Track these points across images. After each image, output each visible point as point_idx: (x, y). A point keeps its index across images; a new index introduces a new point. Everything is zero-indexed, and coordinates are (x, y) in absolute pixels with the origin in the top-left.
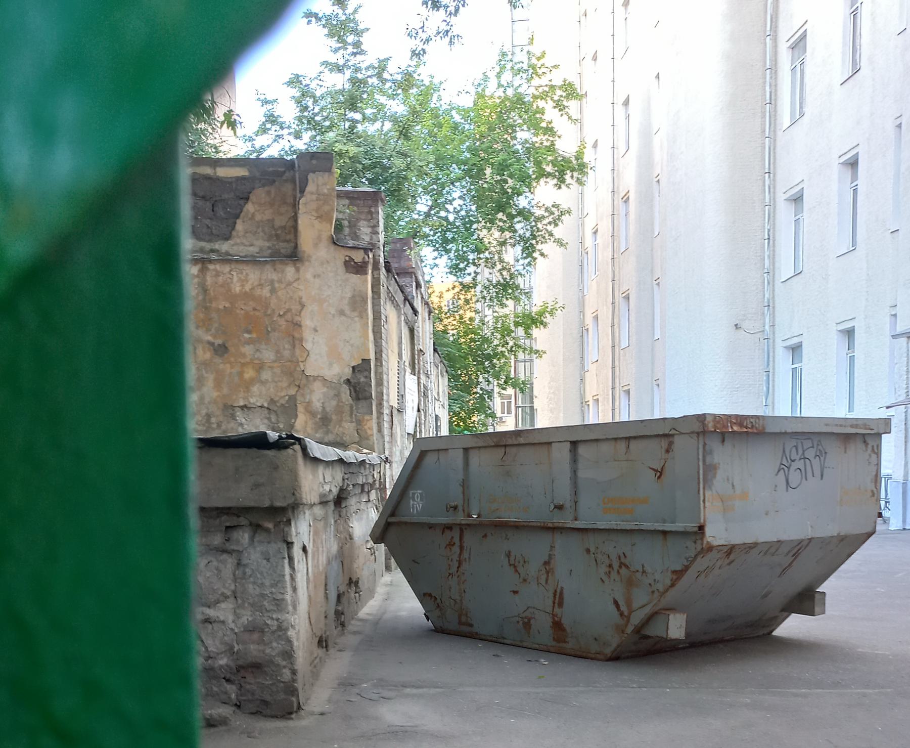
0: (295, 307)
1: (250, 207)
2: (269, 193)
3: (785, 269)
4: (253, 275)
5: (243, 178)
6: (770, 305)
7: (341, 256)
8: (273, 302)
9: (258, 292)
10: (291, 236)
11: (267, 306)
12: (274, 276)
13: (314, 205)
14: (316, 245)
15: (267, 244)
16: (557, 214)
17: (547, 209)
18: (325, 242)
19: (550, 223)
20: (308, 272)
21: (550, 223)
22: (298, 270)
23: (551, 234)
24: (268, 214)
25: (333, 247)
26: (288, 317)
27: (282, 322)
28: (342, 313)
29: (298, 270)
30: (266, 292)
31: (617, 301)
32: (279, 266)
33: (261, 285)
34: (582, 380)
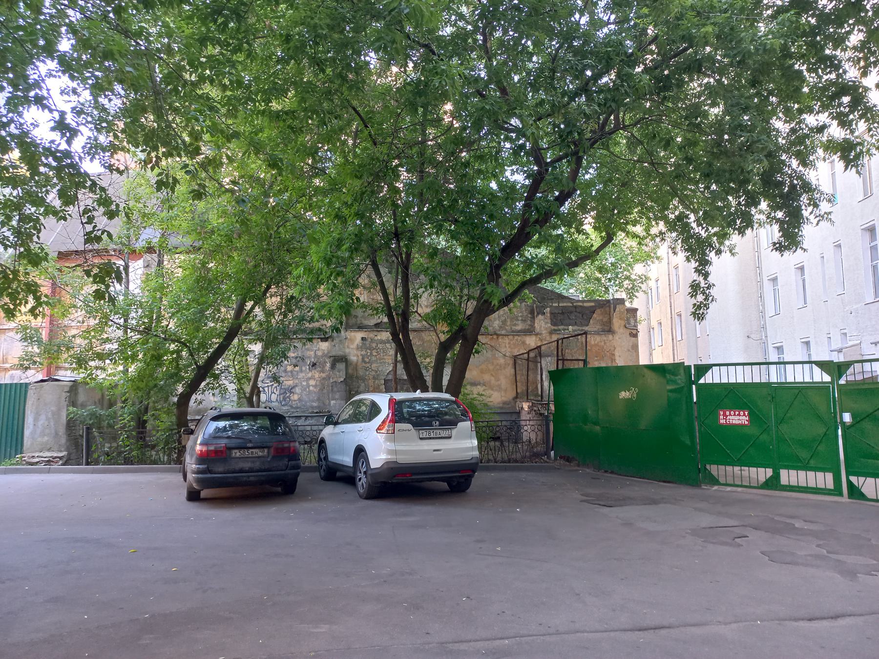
0: (612, 349)
1: (595, 315)
3: (770, 311)
4: (598, 338)
5: (592, 306)
6: (764, 327)
7: (628, 331)
9: (600, 344)
11: (603, 348)
12: (605, 338)
16: (645, 279)
18: (622, 327)
20: (617, 337)
23: (640, 288)
27: (608, 354)
28: (629, 350)
30: (603, 343)
31: (673, 316)
34: (651, 354)
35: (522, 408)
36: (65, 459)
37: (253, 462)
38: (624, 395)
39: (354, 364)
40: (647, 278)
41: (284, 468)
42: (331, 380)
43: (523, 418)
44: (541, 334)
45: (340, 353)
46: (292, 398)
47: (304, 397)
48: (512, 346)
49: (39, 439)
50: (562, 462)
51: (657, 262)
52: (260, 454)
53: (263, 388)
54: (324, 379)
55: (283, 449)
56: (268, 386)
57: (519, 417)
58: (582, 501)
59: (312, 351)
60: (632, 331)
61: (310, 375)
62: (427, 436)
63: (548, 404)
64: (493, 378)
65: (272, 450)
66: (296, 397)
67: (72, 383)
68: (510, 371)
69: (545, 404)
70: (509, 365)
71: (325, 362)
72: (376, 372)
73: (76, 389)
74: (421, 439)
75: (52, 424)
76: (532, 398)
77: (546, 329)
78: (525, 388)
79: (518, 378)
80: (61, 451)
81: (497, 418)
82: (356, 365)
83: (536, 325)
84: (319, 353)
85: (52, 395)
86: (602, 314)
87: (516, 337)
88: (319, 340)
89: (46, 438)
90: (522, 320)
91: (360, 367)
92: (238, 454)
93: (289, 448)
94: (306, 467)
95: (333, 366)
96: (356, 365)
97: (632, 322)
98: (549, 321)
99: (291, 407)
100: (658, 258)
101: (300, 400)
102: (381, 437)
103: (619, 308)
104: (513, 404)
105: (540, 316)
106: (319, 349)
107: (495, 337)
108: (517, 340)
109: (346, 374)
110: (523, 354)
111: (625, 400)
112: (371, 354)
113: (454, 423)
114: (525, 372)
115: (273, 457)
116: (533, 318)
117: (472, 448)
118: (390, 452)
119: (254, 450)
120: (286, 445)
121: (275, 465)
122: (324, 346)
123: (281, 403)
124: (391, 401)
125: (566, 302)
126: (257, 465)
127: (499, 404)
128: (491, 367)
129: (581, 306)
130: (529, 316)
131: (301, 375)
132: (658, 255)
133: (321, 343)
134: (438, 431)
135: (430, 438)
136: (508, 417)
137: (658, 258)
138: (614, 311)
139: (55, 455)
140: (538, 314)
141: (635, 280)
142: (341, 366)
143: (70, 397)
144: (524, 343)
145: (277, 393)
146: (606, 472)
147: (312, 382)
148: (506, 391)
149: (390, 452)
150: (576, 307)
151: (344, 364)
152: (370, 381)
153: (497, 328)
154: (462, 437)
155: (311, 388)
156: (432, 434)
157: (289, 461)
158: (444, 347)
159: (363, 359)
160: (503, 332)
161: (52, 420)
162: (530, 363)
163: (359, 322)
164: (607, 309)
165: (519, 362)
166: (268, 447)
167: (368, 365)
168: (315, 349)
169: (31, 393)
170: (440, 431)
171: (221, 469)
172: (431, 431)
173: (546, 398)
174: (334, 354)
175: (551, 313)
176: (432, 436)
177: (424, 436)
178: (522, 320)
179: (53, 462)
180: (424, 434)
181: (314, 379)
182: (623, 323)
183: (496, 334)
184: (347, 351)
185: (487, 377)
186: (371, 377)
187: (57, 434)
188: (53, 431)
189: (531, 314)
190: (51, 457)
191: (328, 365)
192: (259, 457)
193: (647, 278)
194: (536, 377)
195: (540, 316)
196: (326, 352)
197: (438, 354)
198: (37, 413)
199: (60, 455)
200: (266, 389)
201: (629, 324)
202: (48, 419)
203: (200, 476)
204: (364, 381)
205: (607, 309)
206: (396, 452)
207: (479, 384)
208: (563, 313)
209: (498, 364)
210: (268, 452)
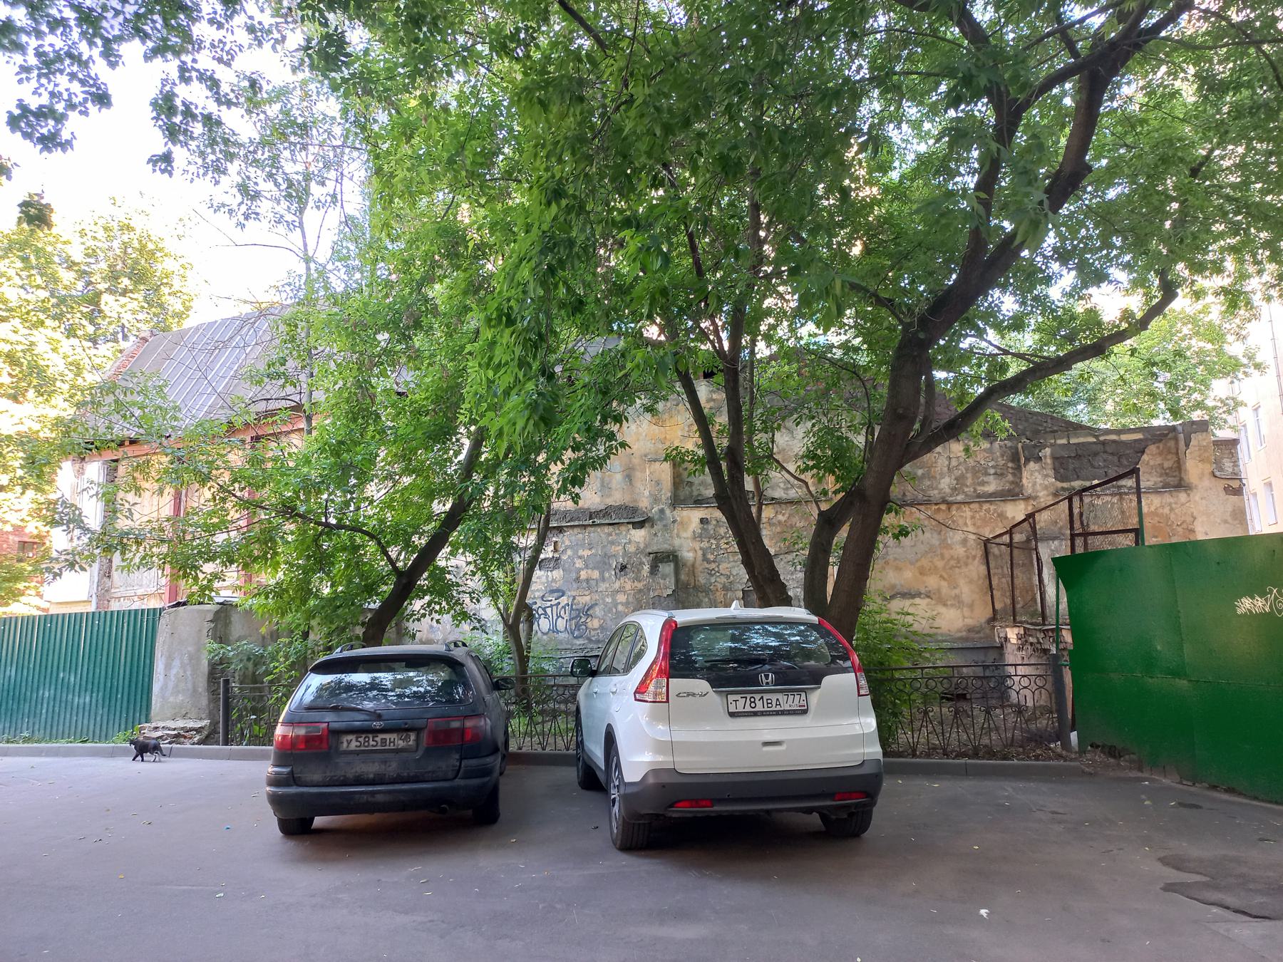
0: (1189, 519)
1: (1145, 457)
2: (1158, 448)
5: (1140, 440)
7: (1223, 483)
8: (1172, 516)
9: (1161, 511)
10: (1177, 473)
12: (1172, 500)
13: (1197, 453)
14: (1201, 479)
15: (1159, 479)
17: (1222, 401)
19: (1224, 412)
20: (1196, 496)
21: (1224, 412)
22: (1189, 495)
23: (1225, 422)
24: (1159, 460)
25: (1214, 479)
26: (1184, 526)
28: (1226, 522)
29: (1189, 495)
30: (1167, 510)
32: (1174, 494)
33: (1163, 507)
35: (1006, 639)
36: (205, 733)
37: (385, 762)
38: (1246, 604)
39: (689, 564)
40: (1238, 404)
41: (450, 775)
42: (652, 594)
43: (1010, 658)
44: (1035, 498)
45: (665, 547)
46: (589, 625)
47: (609, 622)
48: (979, 523)
49: (171, 699)
50: (1099, 757)
51: (1256, 373)
52: (401, 744)
53: (544, 609)
54: (640, 591)
55: (448, 733)
56: (551, 606)
57: (1002, 655)
58: (1170, 888)
59: (619, 544)
60: (1231, 483)
61: (617, 585)
62: (748, 709)
63: (1058, 630)
64: (944, 584)
65: (424, 735)
66: (595, 623)
67: (219, 606)
68: (978, 568)
69: (1052, 630)
70: (974, 557)
71: (642, 563)
72: (728, 577)
73: (228, 617)
74: (732, 715)
75: (189, 673)
76: (1024, 619)
77: (1046, 488)
78: (1008, 601)
79: (995, 582)
80: (201, 719)
81: (954, 660)
82: (693, 566)
83: (1024, 481)
84: (632, 549)
85: (193, 623)
86: (1160, 454)
87: (986, 506)
88: (631, 526)
89: (180, 697)
90: (995, 474)
91: (700, 569)
92: (354, 745)
93: (462, 731)
94: (549, 755)
95: (654, 569)
96: (693, 566)
97: (1228, 465)
98: (1051, 473)
99: (589, 639)
100: (1258, 366)
101: (601, 627)
102: (642, 711)
103: (1196, 439)
104: (987, 631)
105: (1032, 464)
106: (630, 542)
107: (943, 507)
108: (988, 511)
109: (677, 581)
110: (1000, 535)
111: (1250, 616)
112: (718, 546)
113: (815, 679)
114: (1007, 571)
115: (428, 752)
116: (1018, 469)
117: (862, 739)
118: (660, 747)
119: (387, 736)
120: (455, 724)
121: (430, 768)
122: (639, 535)
123: (573, 633)
124: (669, 625)
125: (1086, 436)
126: (392, 768)
127: (959, 630)
128: (940, 564)
129: (1114, 441)
130: (1010, 465)
131: (603, 586)
132: (1258, 360)
133: (633, 532)
134: (774, 697)
135: (755, 714)
136: (979, 657)
137: (1258, 366)
138: (1187, 445)
139: (191, 724)
140: (1027, 460)
141: (1215, 408)
142: (667, 569)
143: (215, 629)
144: (1002, 516)
145: (566, 617)
146: (1214, 787)
147: (621, 598)
148: (971, 606)
149: (660, 747)
150: (1104, 443)
151: (672, 565)
152: (718, 594)
153: (948, 490)
154: (835, 709)
155: (620, 608)
156: (759, 704)
157: (461, 760)
158: (828, 523)
159: (704, 555)
160: (960, 498)
161: (189, 668)
162: (1016, 552)
163: (695, 493)
164: (1172, 444)
165: (995, 550)
166: (418, 730)
167: (713, 566)
168: (624, 541)
169: (163, 626)
170: (780, 696)
171: (317, 777)
172: (757, 697)
173: (1052, 620)
174: (654, 548)
175: (1054, 458)
176: (759, 707)
177: (740, 709)
178: (995, 474)
179: (185, 737)
180: (740, 703)
181: (625, 592)
182: (1208, 468)
183: (944, 501)
184: (677, 542)
185: (932, 582)
186: (720, 586)
187: (195, 691)
188: (190, 686)
189: (1012, 461)
190: (182, 728)
191: (646, 568)
192: (397, 751)
193: (1238, 404)
194: (1030, 579)
195: (1032, 464)
196: (642, 546)
197: (817, 534)
198: (170, 656)
199: (198, 725)
200: (549, 610)
201: (1221, 469)
202: (183, 666)
203: (280, 790)
204: (707, 595)
205: (1172, 444)
206: (671, 747)
207: (918, 595)
208: (1078, 457)
209: (952, 557)
210: (417, 740)
